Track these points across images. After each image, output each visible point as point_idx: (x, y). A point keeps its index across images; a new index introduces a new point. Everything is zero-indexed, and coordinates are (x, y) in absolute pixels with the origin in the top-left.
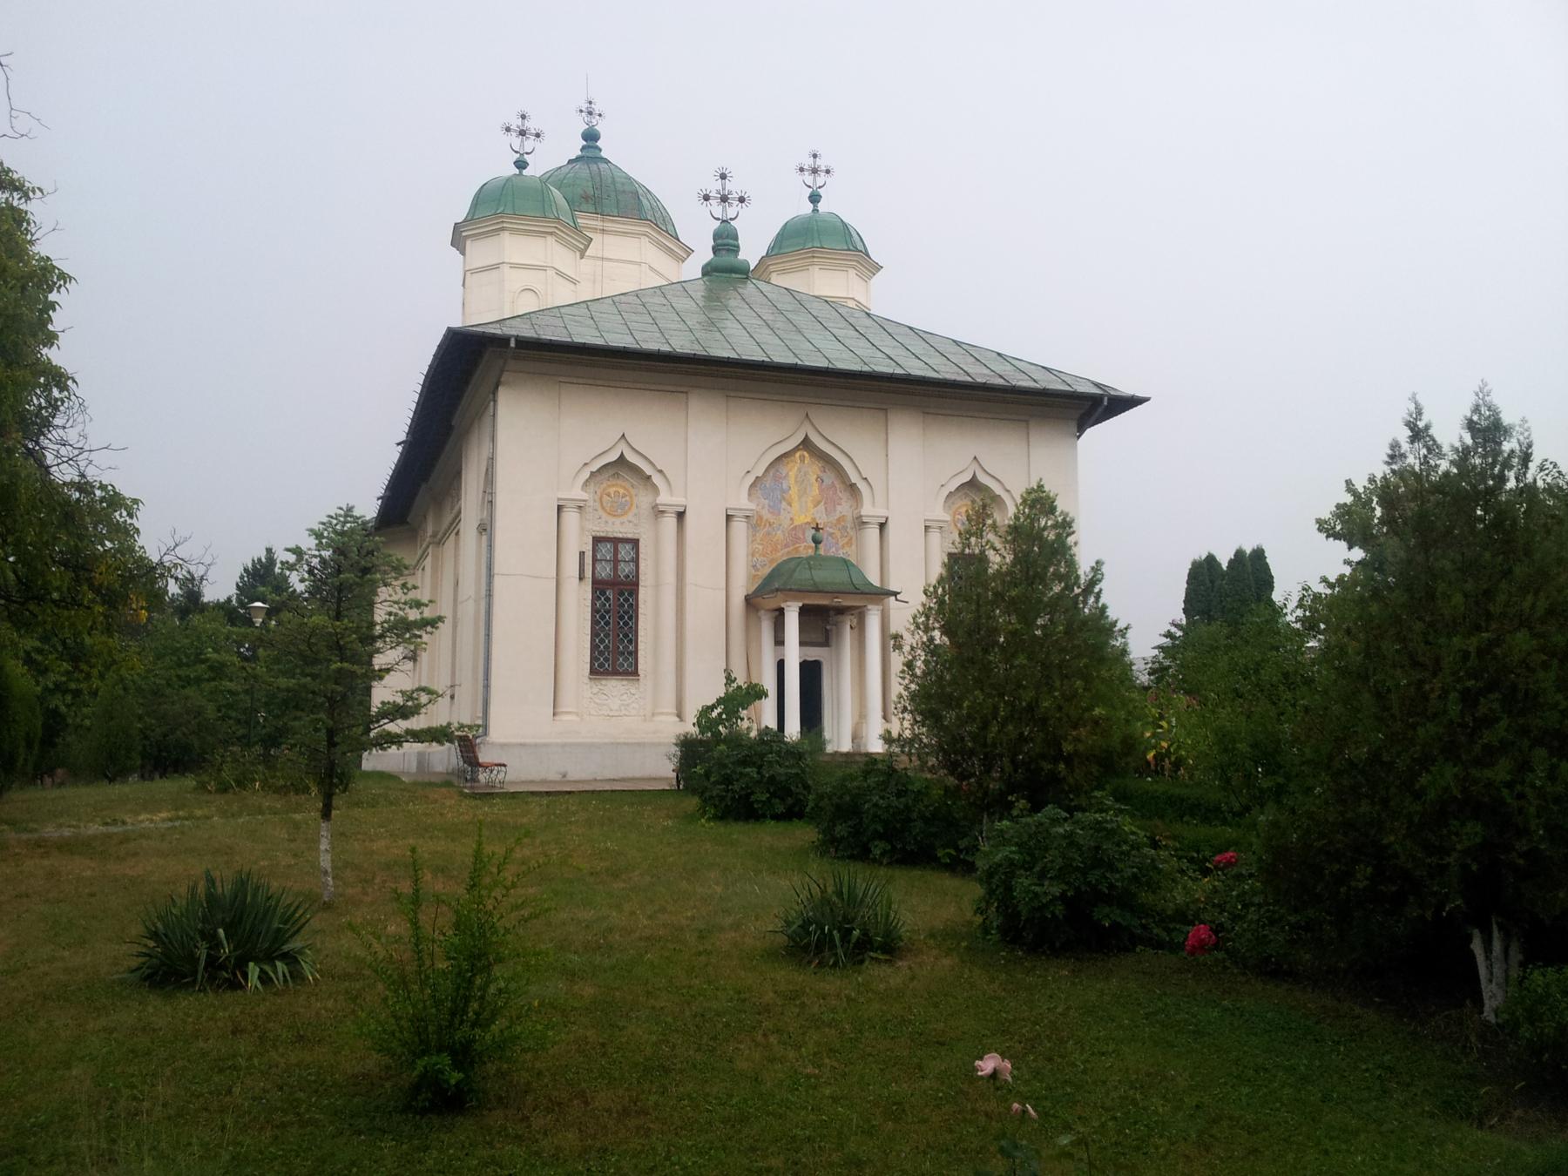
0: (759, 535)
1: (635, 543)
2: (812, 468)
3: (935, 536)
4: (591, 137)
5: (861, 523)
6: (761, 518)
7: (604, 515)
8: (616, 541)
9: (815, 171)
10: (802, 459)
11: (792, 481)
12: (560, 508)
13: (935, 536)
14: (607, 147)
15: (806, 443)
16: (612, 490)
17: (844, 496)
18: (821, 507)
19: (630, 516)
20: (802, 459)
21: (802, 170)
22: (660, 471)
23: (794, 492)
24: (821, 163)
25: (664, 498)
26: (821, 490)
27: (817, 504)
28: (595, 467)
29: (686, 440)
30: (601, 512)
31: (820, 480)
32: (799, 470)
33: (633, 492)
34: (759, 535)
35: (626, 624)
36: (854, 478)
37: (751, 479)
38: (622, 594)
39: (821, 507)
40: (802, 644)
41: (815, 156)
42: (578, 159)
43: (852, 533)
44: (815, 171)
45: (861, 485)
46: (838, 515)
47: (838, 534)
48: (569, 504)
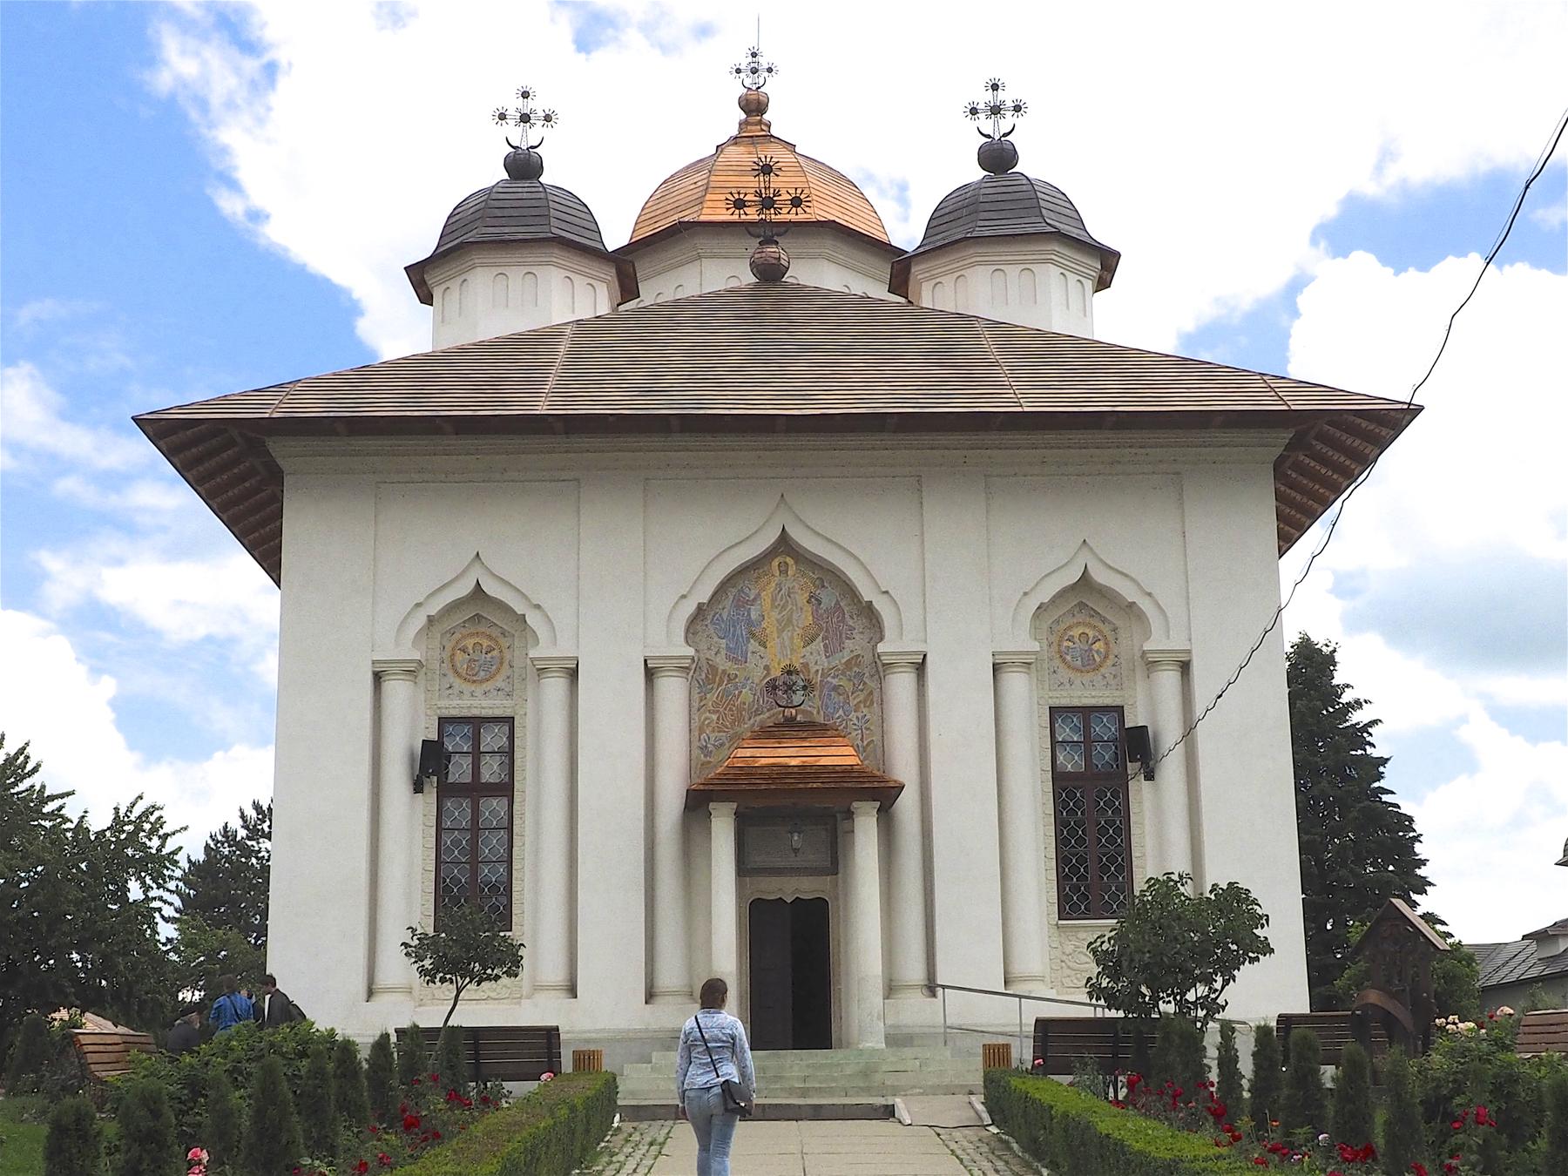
0: (712, 697)
1: (510, 721)
2: (797, 583)
3: (1017, 684)
4: (754, 106)
5: (881, 669)
7: (457, 682)
8: (1086, 712)
10: (783, 569)
13: (1017, 684)
14: (779, 120)
15: (784, 544)
16: (469, 643)
17: (858, 624)
18: (818, 645)
19: (499, 681)
20: (783, 569)
22: (538, 607)
25: (1156, 642)
28: (434, 608)
30: (452, 678)
31: (814, 599)
32: (779, 586)
33: (504, 642)
34: (712, 697)
35: (1111, 841)
36: (867, 593)
37: (689, 608)
38: (1101, 794)
39: (818, 645)
40: (743, 869)
42: (735, 141)
43: (872, 684)
44: (996, 110)
45: (881, 605)
47: (849, 687)
48: (395, 668)
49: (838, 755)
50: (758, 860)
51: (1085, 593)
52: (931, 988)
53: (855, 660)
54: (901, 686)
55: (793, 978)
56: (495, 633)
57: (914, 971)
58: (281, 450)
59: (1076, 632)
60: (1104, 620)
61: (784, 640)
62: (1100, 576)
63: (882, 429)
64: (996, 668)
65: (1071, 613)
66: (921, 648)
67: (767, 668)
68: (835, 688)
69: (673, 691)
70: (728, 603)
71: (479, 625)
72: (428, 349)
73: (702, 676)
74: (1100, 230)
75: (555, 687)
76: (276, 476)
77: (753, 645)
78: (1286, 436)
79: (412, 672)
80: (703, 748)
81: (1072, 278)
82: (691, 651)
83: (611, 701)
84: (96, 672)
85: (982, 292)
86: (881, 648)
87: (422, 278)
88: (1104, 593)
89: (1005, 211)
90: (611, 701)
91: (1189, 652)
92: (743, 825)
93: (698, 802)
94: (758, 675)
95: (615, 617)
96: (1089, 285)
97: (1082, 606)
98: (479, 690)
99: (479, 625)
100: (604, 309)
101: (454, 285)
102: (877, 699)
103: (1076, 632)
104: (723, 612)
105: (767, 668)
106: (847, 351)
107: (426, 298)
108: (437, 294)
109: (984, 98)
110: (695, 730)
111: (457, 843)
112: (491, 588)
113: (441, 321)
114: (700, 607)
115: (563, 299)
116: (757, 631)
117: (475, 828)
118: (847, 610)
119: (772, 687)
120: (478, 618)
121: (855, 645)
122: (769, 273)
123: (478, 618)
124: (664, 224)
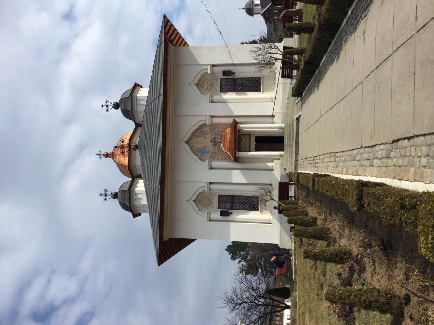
2: (195, 140)
3: (215, 98)
4: (107, 155)
5: (212, 124)
6: (211, 156)
9: (106, 195)
11: (199, 146)
12: (210, 221)
16: (204, 203)
17: (203, 128)
18: (207, 136)
21: (107, 110)
23: (202, 145)
24: (103, 193)
26: (201, 136)
27: (206, 138)
29: (186, 116)
30: (211, 206)
37: (199, 161)
39: (207, 136)
40: (249, 151)
41: (103, 106)
42: (113, 159)
43: (215, 126)
44: (107, 106)
45: (200, 124)
46: (209, 131)
49: (228, 130)
50: (247, 149)
51: (199, 85)
52: (273, 116)
53: (210, 129)
54: (215, 120)
55: (271, 142)
56: (202, 198)
57: (270, 119)
58: (166, 238)
59: (206, 87)
60: (204, 81)
61: (206, 142)
62: (196, 81)
63: (165, 144)
64: (212, 102)
65: (202, 88)
66: (208, 116)
67: (211, 146)
68: (215, 133)
69: (215, 164)
70: (198, 153)
71: (201, 200)
72: (148, 214)
73: (213, 158)
74: (131, 87)
75: (213, 186)
76: (171, 239)
77: (206, 149)
78: (169, 44)
79: (209, 214)
80: (226, 159)
81: (140, 92)
82: (207, 161)
83: (217, 176)
84: (233, 258)
85: (141, 107)
86: (208, 124)
87: (136, 215)
88: (199, 81)
89: (126, 106)
90: (217, 176)
91: (211, 65)
92: (240, 151)
93: (237, 160)
94: (212, 148)
95: (202, 174)
96: (141, 89)
97: (201, 86)
98: (213, 201)
99: (201, 200)
100: (142, 181)
101: (137, 208)
102: (218, 125)
103: (206, 87)
104: (201, 154)
105: (211, 146)
106: (151, 130)
107: (140, 214)
108: (140, 212)
109: (105, 108)
110: (222, 160)
111: (242, 206)
112: (194, 198)
113: (144, 211)
114: (199, 159)
115: (140, 186)
116: (204, 148)
117: (240, 203)
118: (201, 130)
119: (214, 145)
120: (199, 201)
121: (207, 129)
122: (136, 147)
123: (199, 201)
124: (129, 172)
